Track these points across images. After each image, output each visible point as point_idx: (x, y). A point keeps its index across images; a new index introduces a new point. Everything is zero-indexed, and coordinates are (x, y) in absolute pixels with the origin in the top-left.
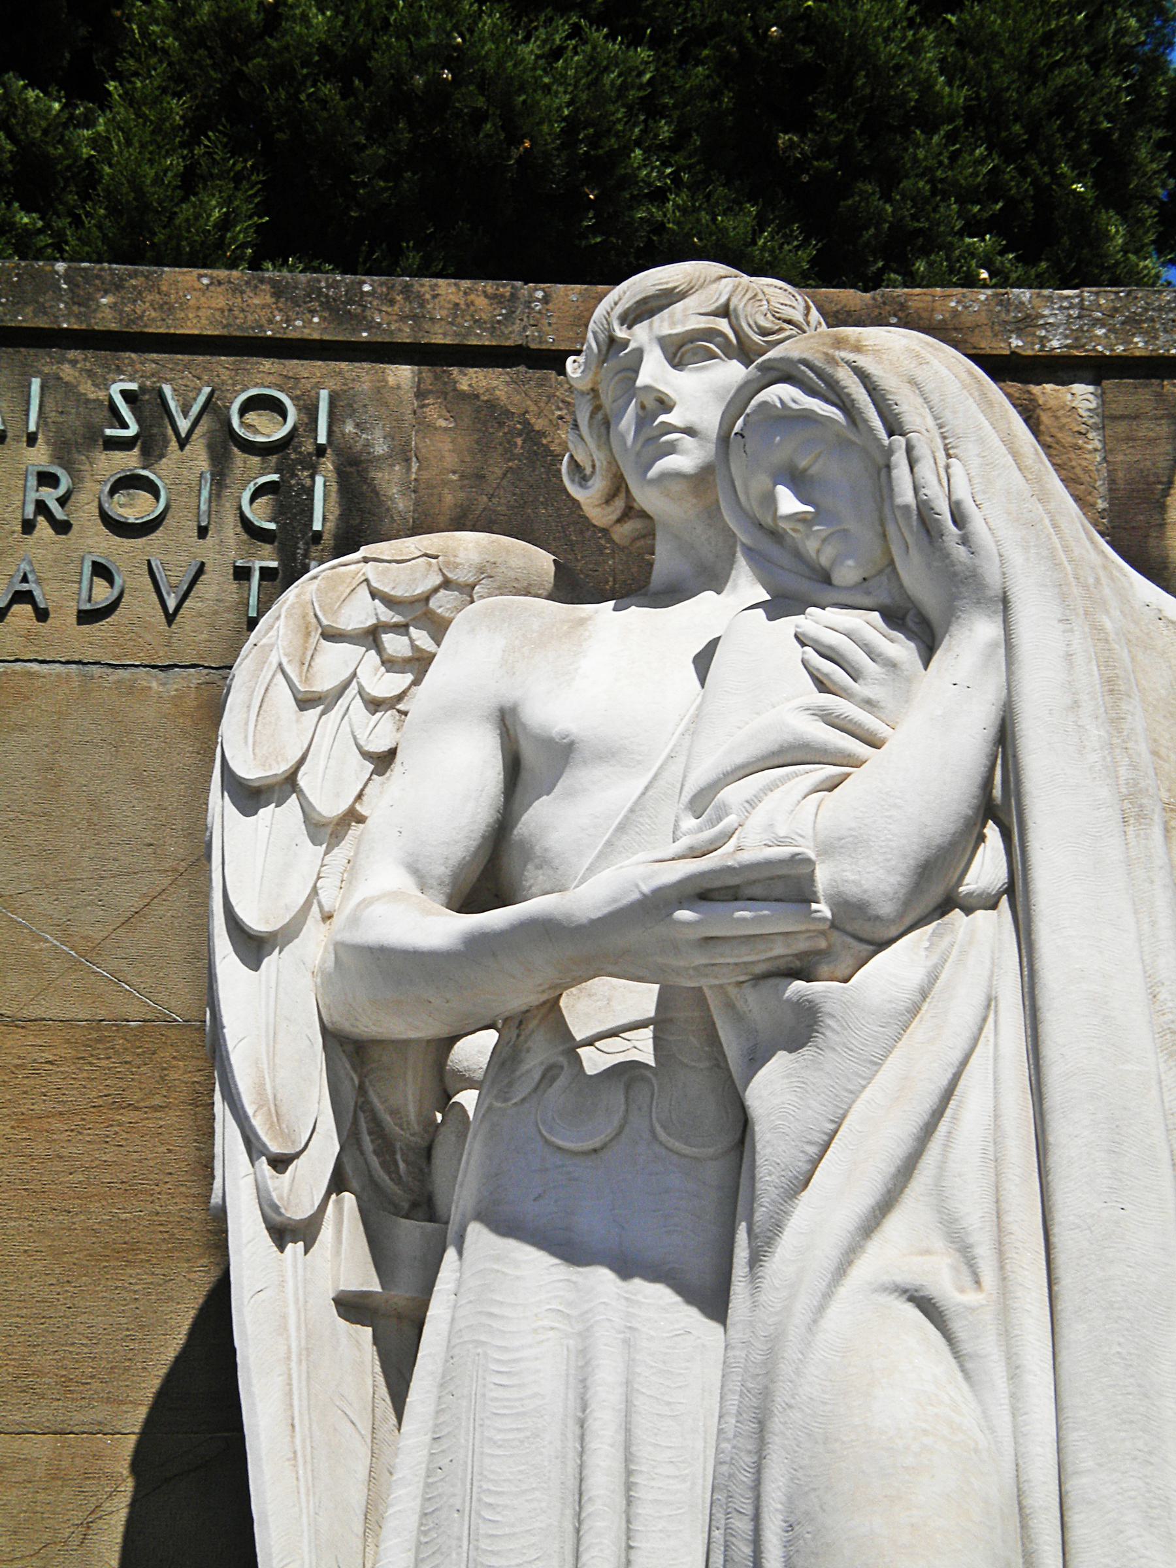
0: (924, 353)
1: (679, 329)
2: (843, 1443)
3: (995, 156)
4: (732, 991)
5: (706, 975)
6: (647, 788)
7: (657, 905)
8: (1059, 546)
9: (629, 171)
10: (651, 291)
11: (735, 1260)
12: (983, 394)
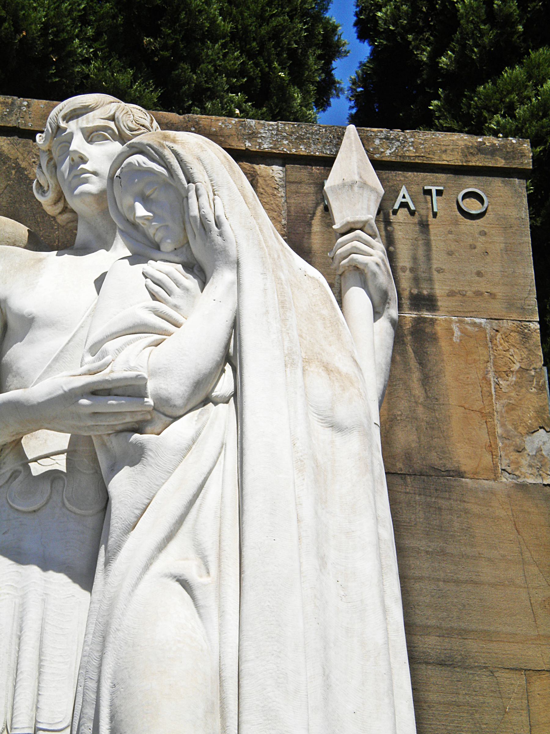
0: (204, 146)
1: (91, 125)
2: (141, 646)
3: (244, 56)
4: (106, 438)
5: (93, 430)
6: (69, 341)
7: (71, 397)
8: (262, 239)
9: (73, 49)
10: (78, 106)
11: (98, 562)
12: (231, 167)
